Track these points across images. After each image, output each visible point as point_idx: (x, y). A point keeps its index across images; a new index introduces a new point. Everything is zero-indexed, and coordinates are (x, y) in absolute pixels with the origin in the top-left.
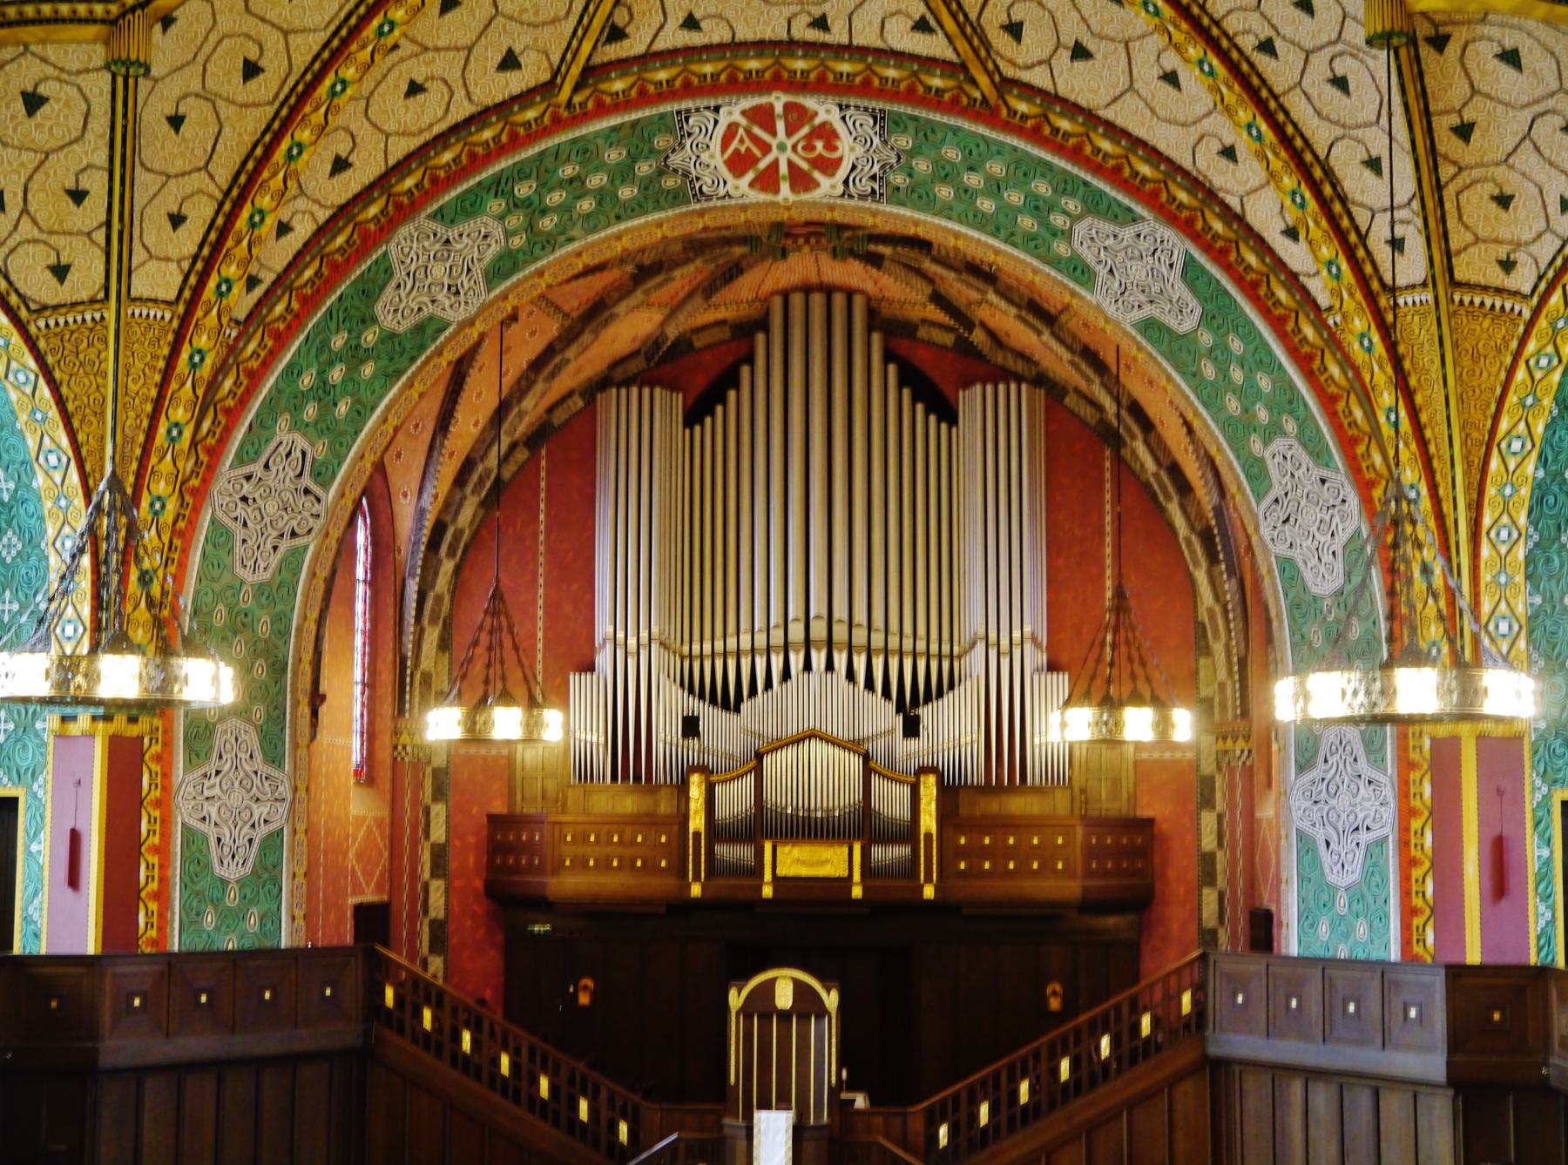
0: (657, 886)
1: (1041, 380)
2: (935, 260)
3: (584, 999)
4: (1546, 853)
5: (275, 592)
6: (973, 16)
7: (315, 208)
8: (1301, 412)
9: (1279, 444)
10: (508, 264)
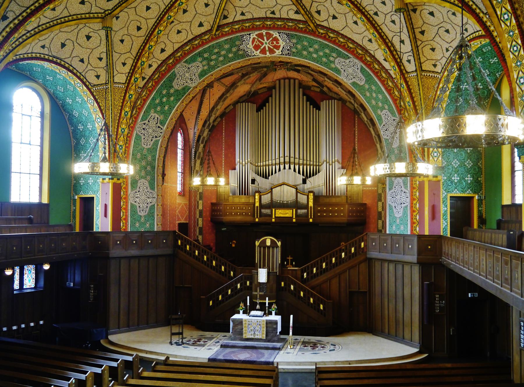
0: (249, 219)
1: (340, 99)
2: (311, 70)
3: (233, 245)
4: (446, 209)
5: (152, 151)
6: (308, 9)
7: (157, 61)
8: (388, 104)
9: (384, 111)
10: (204, 73)
